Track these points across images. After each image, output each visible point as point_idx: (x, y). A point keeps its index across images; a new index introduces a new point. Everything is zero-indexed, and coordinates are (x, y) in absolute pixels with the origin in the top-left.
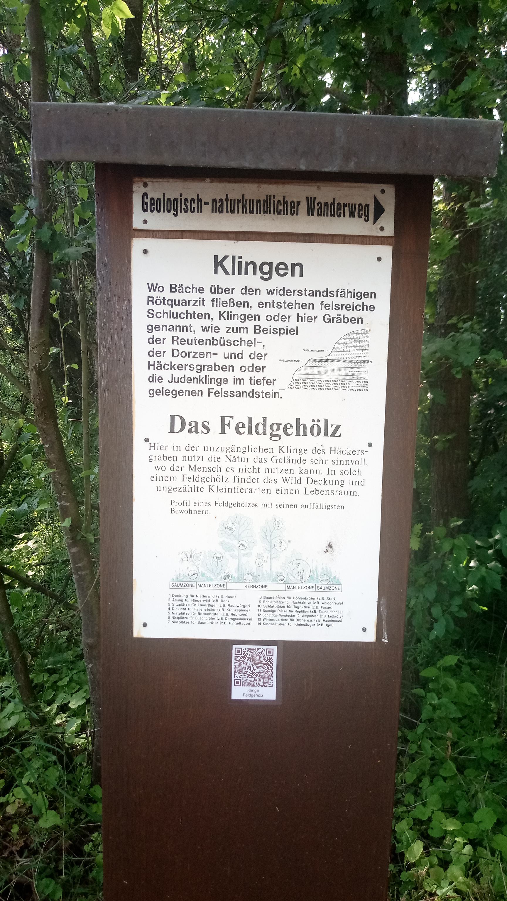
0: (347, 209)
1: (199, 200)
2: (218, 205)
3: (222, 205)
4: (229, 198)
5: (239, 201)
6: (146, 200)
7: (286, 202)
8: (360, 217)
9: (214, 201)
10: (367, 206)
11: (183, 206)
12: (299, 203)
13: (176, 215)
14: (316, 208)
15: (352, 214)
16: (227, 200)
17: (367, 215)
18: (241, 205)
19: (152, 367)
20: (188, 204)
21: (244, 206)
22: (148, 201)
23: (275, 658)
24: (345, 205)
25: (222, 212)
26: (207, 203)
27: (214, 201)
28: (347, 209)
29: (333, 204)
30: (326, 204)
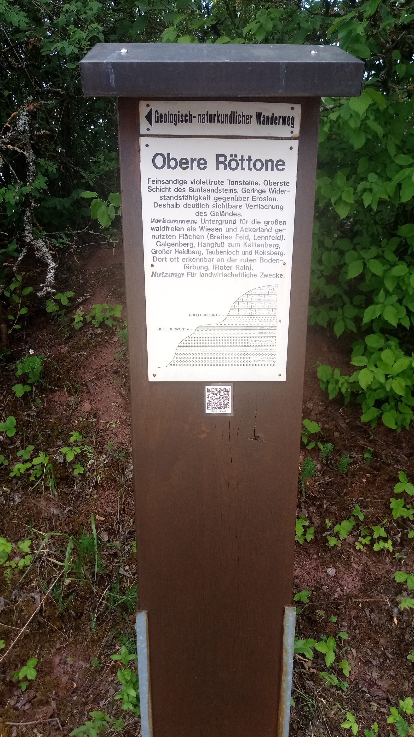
0: (281, 120)
1: (190, 115)
2: (202, 118)
3: (204, 118)
4: (209, 113)
5: (215, 115)
6: (157, 115)
7: (243, 116)
8: (289, 125)
9: (199, 115)
10: (157, 122)
11: (181, 119)
12: (251, 116)
13: (176, 125)
14: (262, 119)
15: (284, 123)
16: (207, 114)
17: (293, 124)
18: (216, 118)
19: (200, 245)
20: (184, 118)
21: (218, 118)
22: (159, 115)
23: (230, 393)
24: (280, 117)
25: (204, 122)
26: (195, 117)
27: (199, 115)
28: (281, 120)
29: (272, 117)
30: (268, 117)
